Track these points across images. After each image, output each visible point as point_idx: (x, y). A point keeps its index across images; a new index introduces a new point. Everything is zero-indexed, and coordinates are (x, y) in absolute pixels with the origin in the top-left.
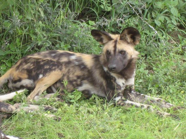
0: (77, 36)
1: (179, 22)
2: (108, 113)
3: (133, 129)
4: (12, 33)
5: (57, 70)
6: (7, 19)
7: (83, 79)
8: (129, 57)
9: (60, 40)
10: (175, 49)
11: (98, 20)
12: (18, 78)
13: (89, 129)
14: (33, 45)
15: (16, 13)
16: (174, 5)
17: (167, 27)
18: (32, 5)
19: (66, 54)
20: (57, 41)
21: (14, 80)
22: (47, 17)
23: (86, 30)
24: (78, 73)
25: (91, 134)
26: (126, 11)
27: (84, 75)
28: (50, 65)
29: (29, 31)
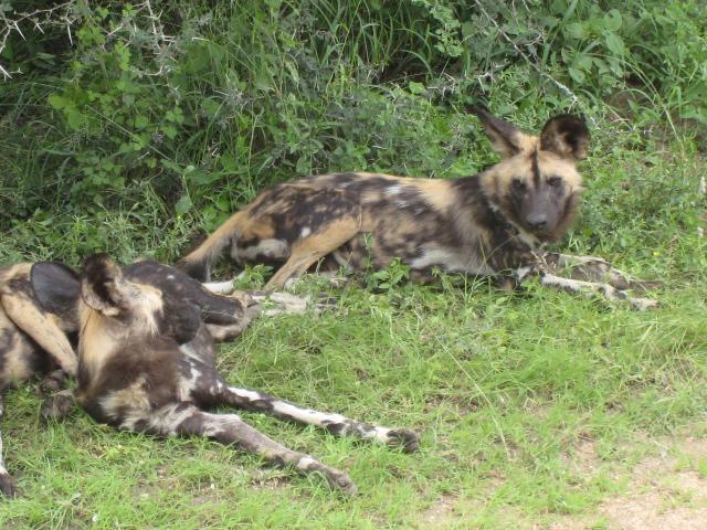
0: (383, 123)
1: (629, 69)
2: (474, 310)
3: (537, 346)
4: (224, 127)
5: (345, 216)
6: (209, 92)
7: (424, 240)
8: (567, 193)
9: (341, 135)
10: (623, 138)
11: (430, 78)
12: (252, 237)
13: (432, 353)
14: (278, 153)
15: (231, 77)
16: (612, 27)
17: (600, 83)
18: (269, 56)
19: (374, 184)
20: (335, 138)
21: (242, 240)
22: (308, 82)
23: (404, 107)
24: (408, 226)
25: (438, 366)
26: (497, 53)
27: (425, 230)
28: (328, 204)
29: (265, 117)
